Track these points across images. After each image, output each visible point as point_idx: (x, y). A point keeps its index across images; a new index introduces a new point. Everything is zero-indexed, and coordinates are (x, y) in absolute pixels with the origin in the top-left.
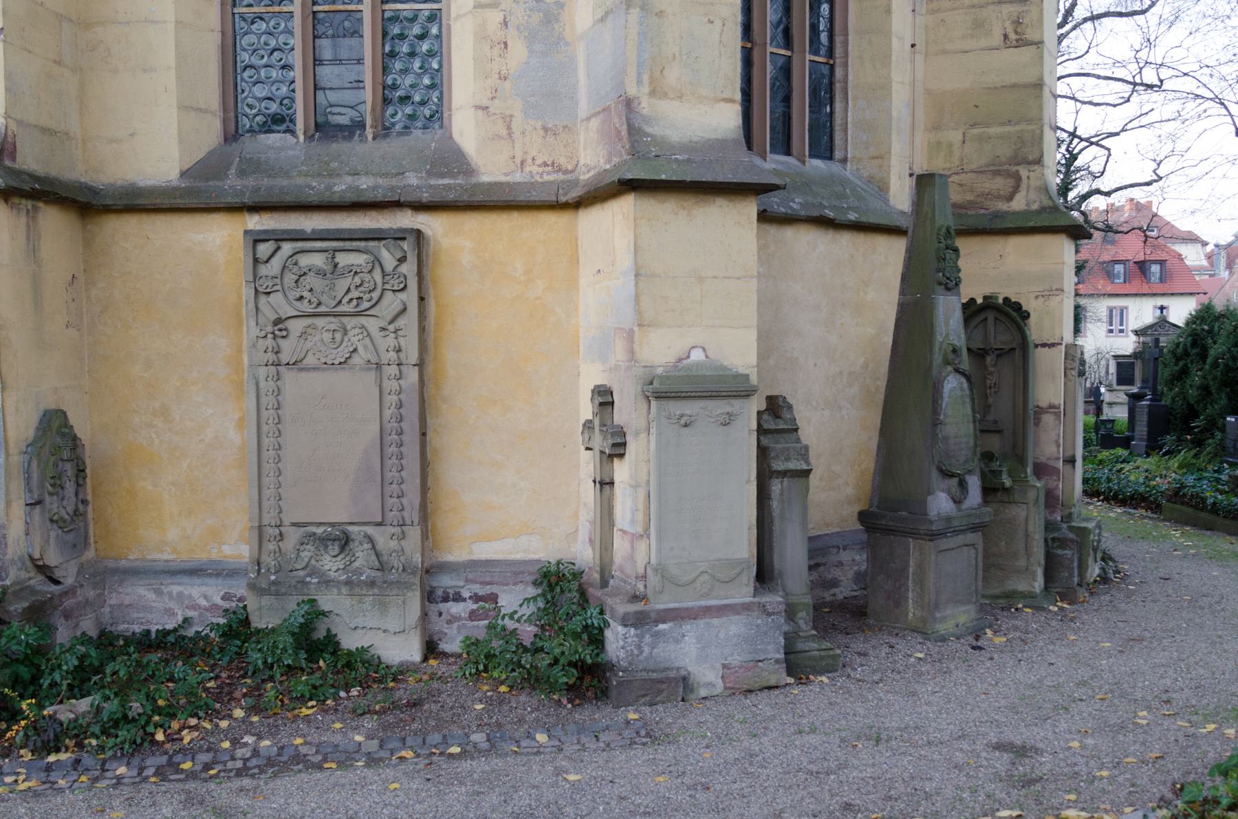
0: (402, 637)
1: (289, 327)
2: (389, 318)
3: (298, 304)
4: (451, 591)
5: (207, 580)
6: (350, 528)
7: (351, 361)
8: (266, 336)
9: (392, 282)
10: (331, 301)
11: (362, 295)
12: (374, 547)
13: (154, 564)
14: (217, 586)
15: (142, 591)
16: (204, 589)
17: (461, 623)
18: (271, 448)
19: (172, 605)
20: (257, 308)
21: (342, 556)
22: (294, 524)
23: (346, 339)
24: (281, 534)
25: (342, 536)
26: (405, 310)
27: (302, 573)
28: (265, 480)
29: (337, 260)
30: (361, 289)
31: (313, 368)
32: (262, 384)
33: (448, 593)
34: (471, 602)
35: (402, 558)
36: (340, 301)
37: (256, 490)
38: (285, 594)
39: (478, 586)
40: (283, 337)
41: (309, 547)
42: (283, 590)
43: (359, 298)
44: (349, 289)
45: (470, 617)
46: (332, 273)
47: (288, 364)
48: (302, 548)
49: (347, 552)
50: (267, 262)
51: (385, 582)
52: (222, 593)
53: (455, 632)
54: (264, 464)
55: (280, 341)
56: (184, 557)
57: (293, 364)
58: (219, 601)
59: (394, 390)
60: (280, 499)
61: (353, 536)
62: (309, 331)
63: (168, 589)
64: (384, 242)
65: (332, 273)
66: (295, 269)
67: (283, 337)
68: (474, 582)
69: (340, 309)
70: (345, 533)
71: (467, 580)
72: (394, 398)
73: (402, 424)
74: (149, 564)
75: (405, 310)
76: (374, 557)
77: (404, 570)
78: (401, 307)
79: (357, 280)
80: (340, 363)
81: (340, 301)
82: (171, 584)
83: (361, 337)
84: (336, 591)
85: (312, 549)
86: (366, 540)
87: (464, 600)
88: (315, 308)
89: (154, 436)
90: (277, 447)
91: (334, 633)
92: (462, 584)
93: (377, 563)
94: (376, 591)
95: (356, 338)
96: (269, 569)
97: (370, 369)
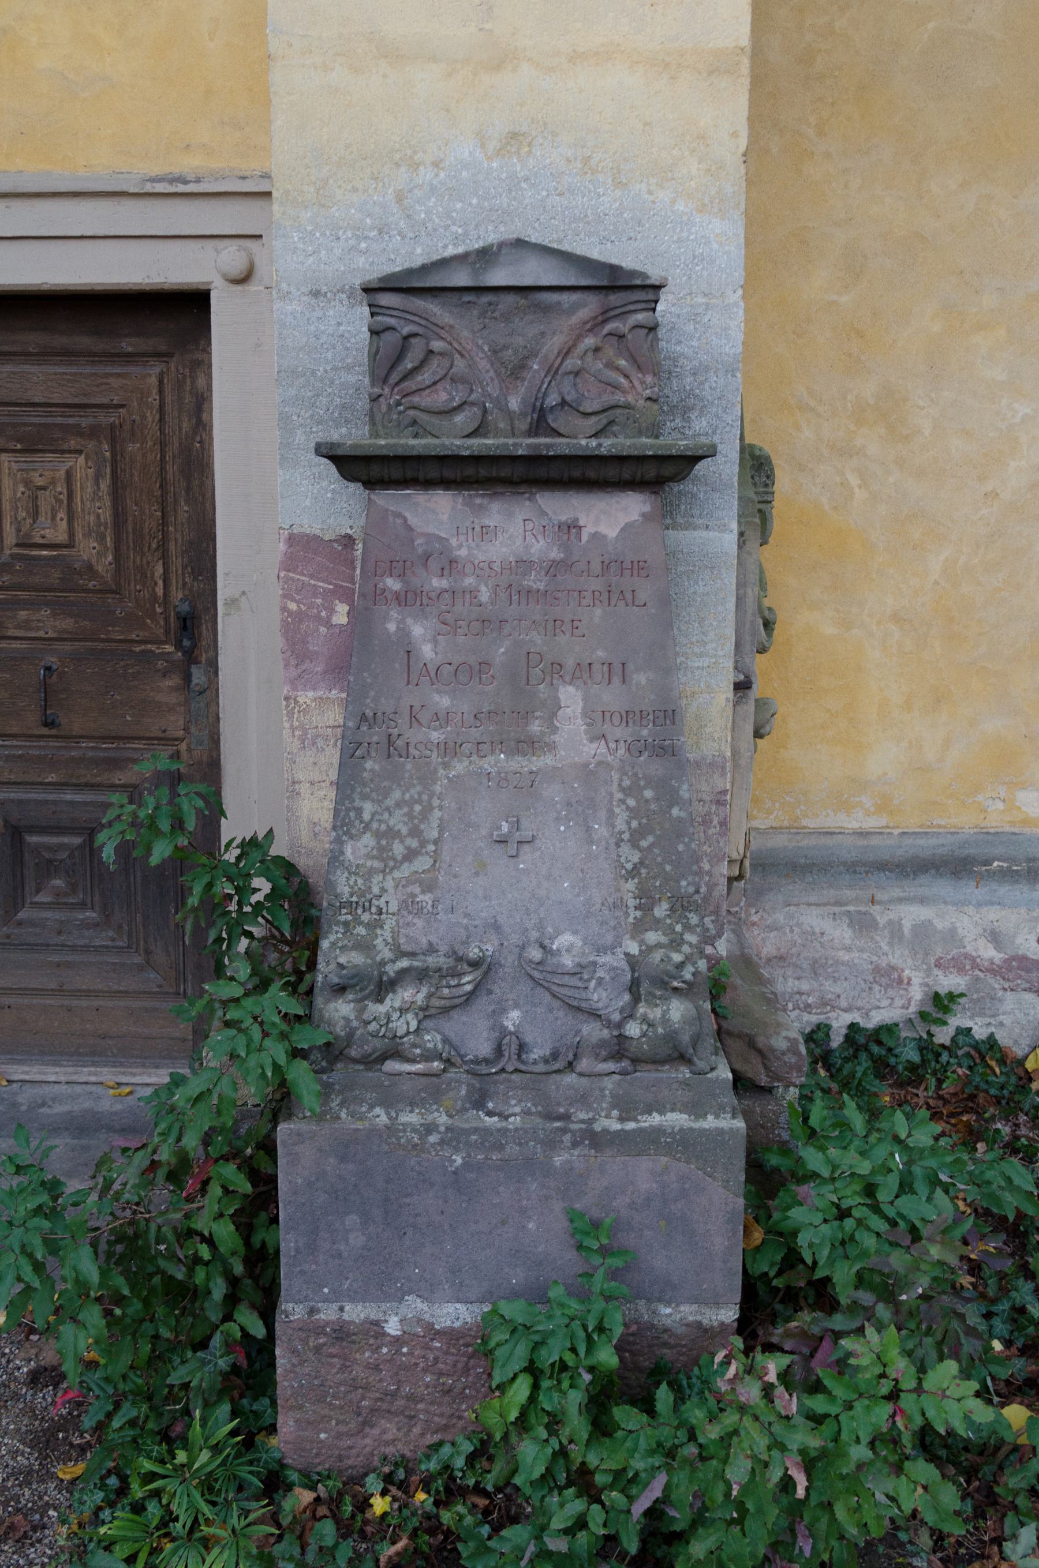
5: (1003, 890)
13: (829, 841)
15: (813, 919)
16: (993, 914)
19: (897, 957)
56: (912, 823)
63: (892, 915)
74: (813, 841)
82: (900, 900)
89: (854, 481)
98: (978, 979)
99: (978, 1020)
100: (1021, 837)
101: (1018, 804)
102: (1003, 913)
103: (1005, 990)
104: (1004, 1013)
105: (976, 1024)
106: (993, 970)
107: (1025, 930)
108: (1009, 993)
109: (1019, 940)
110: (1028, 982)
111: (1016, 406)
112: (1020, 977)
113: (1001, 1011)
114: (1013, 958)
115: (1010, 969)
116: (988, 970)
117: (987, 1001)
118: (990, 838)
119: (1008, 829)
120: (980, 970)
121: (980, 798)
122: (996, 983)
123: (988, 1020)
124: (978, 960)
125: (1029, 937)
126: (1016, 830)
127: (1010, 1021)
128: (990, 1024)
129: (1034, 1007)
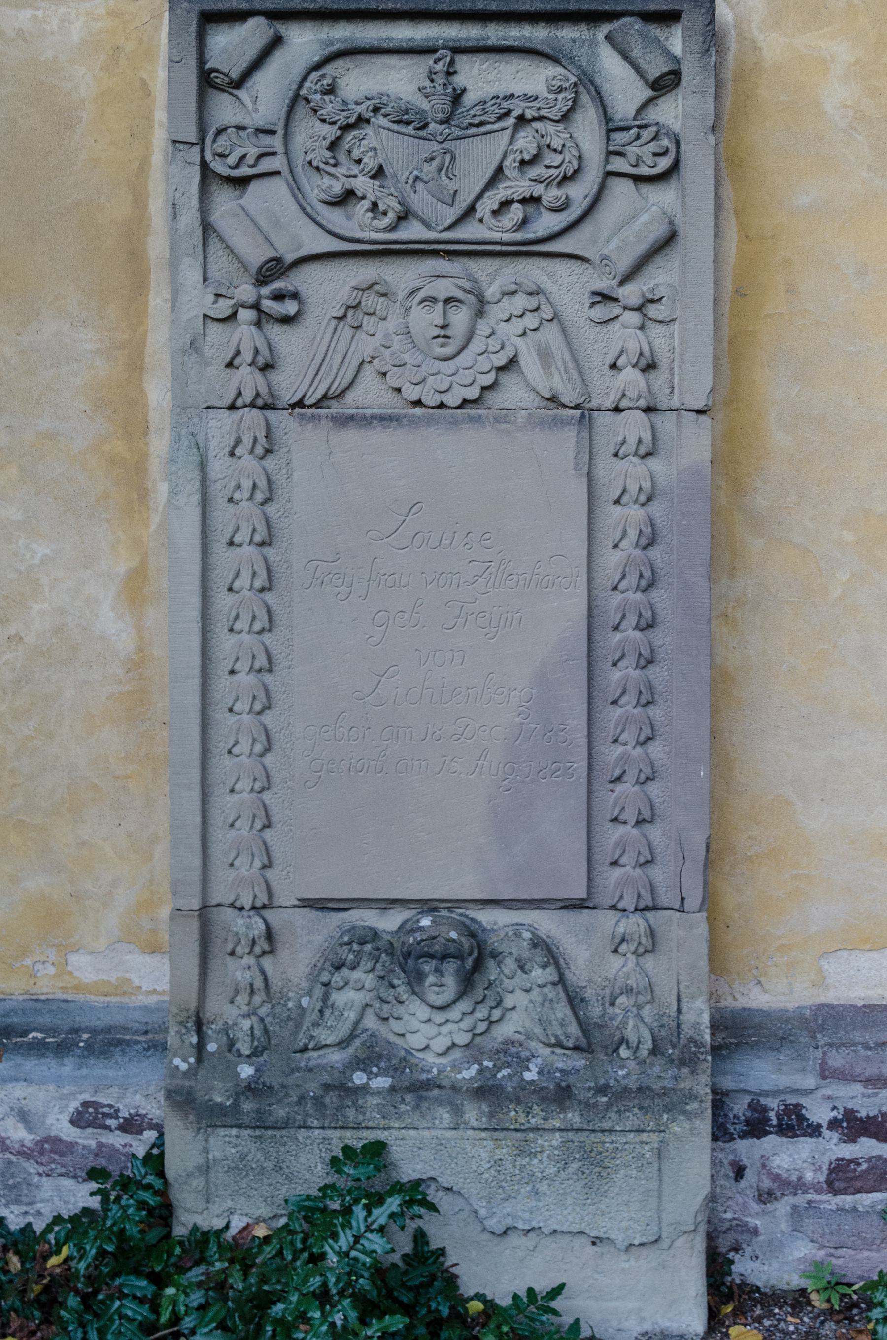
0: (651, 1256)
1: (303, 290)
2: (624, 263)
3: (335, 218)
4: (773, 1103)
5: (30, 1065)
6: (486, 917)
7: (495, 399)
8: (233, 316)
9: (632, 150)
10: (442, 208)
11: (538, 190)
12: (562, 981)
14: (59, 1082)
16: (18, 1091)
17: (801, 1200)
18: (243, 666)
20: (207, 228)
21: (464, 1005)
22: (308, 904)
23: (483, 328)
24: (269, 935)
25: (466, 943)
26: (670, 239)
27: (336, 1057)
28: (222, 765)
29: (459, 80)
30: (534, 172)
31: (382, 418)
32: (219, 466)
33: (765, 1109)
34: (835, 1136)
35: (646, 1011)
36: (471, 210)
37: (195, 795)
38: (285, 1125)
39: (857, 1088)
40: (286, 320)
41: (357, 975)
42: (281, 1112)
43: (534, 200)
44: (500, 170)
45: (830, 1183)
46: (446, 121)
47: (300, 404)
48: (337, 979)
49: (479, 993)
50: (239, 84)
51: (602, 1090)
52: (74, 1105)
53: (784, 1226)
54: (219, 715)
55: (275, 331)
57: (317, 405)
58: (68, 1132)
59: (633, 489)
60: (268, 825)
61: (494, 942)
62: (370, 301)
64: (606, 28)
65: (446, 121)
66: (329, 108)
67: (286, 320)
68: (845, 1076)
69: (470, 231)
70: (472, 932)
71: (826, 1073)
72: (635, 514)
73: (655, 595)
75: (670, 239)
76: (563, 1011)
77: (655, 1051)
78: (659, 231)
79: (526, 142)
80: (465, 403)
81: (471, 210)
83: (531, 321)
84: (445, 1115)
85: (369, 980)
86: (540, 956)
87: (815, 1131)
88: (392, 228)
90: (261, 661)
91: (435, 1245)
92: (810, 1082)
93: (573, 1029)
94: (574, 1117)
95: (518, 326)
96: (231, 1044)
97: (557, 422)
98: (10, 1163)
99: (13, 1208)
100: (72, 1004)
101: (69, 968)
102: (30, 1090)
103: (40, 1175)
104: (42, 1201)
105: (12, 1212)
106: (24, 1152)
107: (56, 1109)
108: (45, 1179)
109: (50, 1120)
110: (63, 1166)
111: (34, 546)
112: (54, 1161)
113: (38, 1199)
114: (47, 1140)
115: (42, 1152)
116: (19, 1153)
117: (24, 1186)
118: (39, 1005)
119: (61, 996)
120: (11, 1153)
121: (28, 962)
122: (31, 1168)
123: (24, 1208)
124: (8, 1142)
125: (60, 1117)
126: (69, 998)
127: (48, 1209)
128: (26, 1213)
129: (74, 1195)
